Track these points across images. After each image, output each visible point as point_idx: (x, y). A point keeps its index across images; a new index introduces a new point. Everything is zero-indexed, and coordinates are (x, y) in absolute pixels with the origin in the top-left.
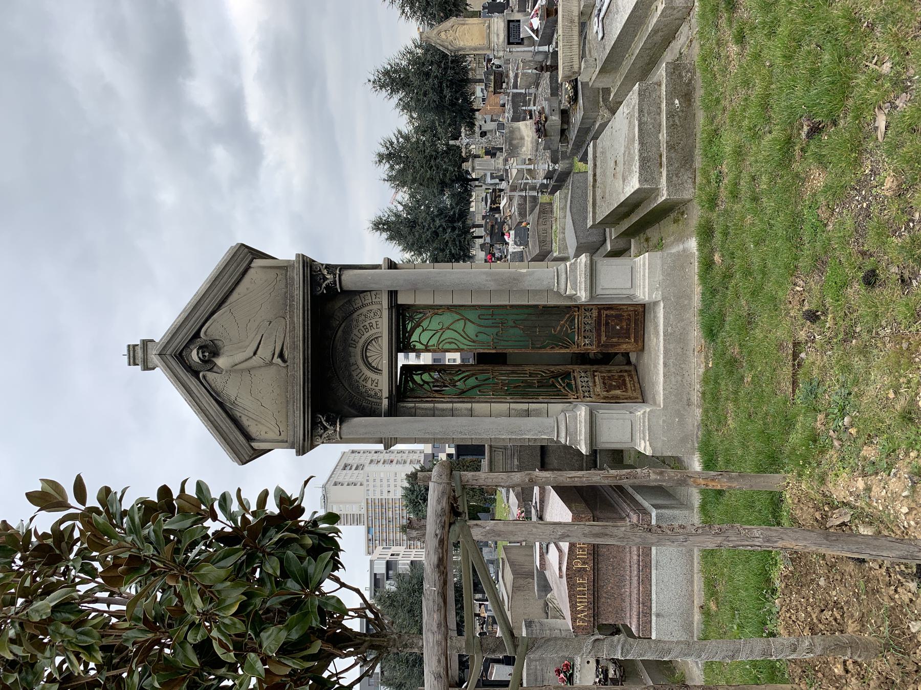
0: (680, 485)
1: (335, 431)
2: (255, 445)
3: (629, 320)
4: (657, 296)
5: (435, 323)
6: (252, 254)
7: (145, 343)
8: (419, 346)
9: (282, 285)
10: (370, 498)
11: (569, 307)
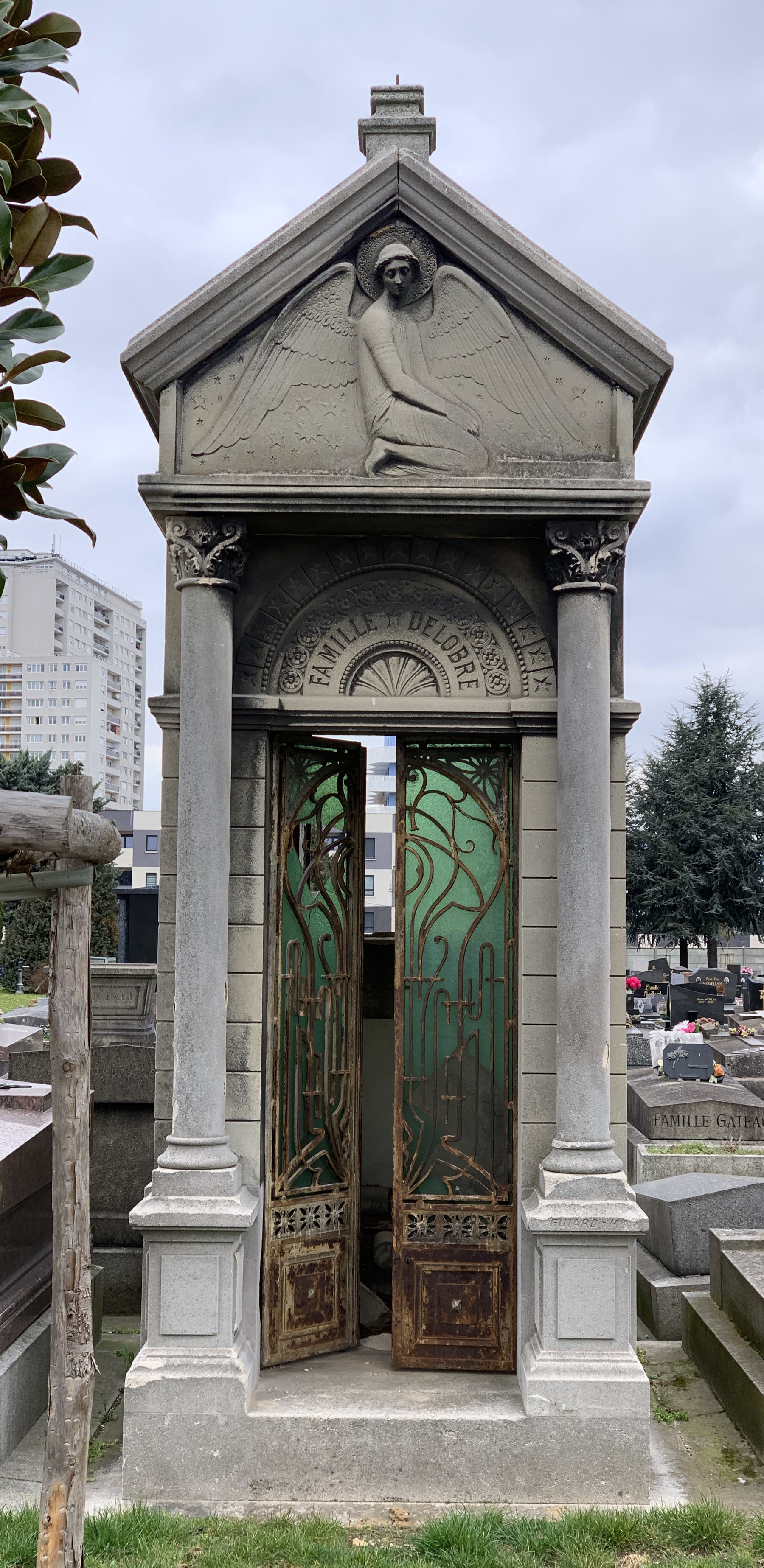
0: (51, 1456)
1: (200, 574)
2: (170, 395)
3: (472, 1328)
4: (537, 1404)
5: (472, 832)
6: (647, 393)
7: (427, 130)
8: (413, 789)
9: (572, 447)
10: (24, 671)
11: (509, 1178)
